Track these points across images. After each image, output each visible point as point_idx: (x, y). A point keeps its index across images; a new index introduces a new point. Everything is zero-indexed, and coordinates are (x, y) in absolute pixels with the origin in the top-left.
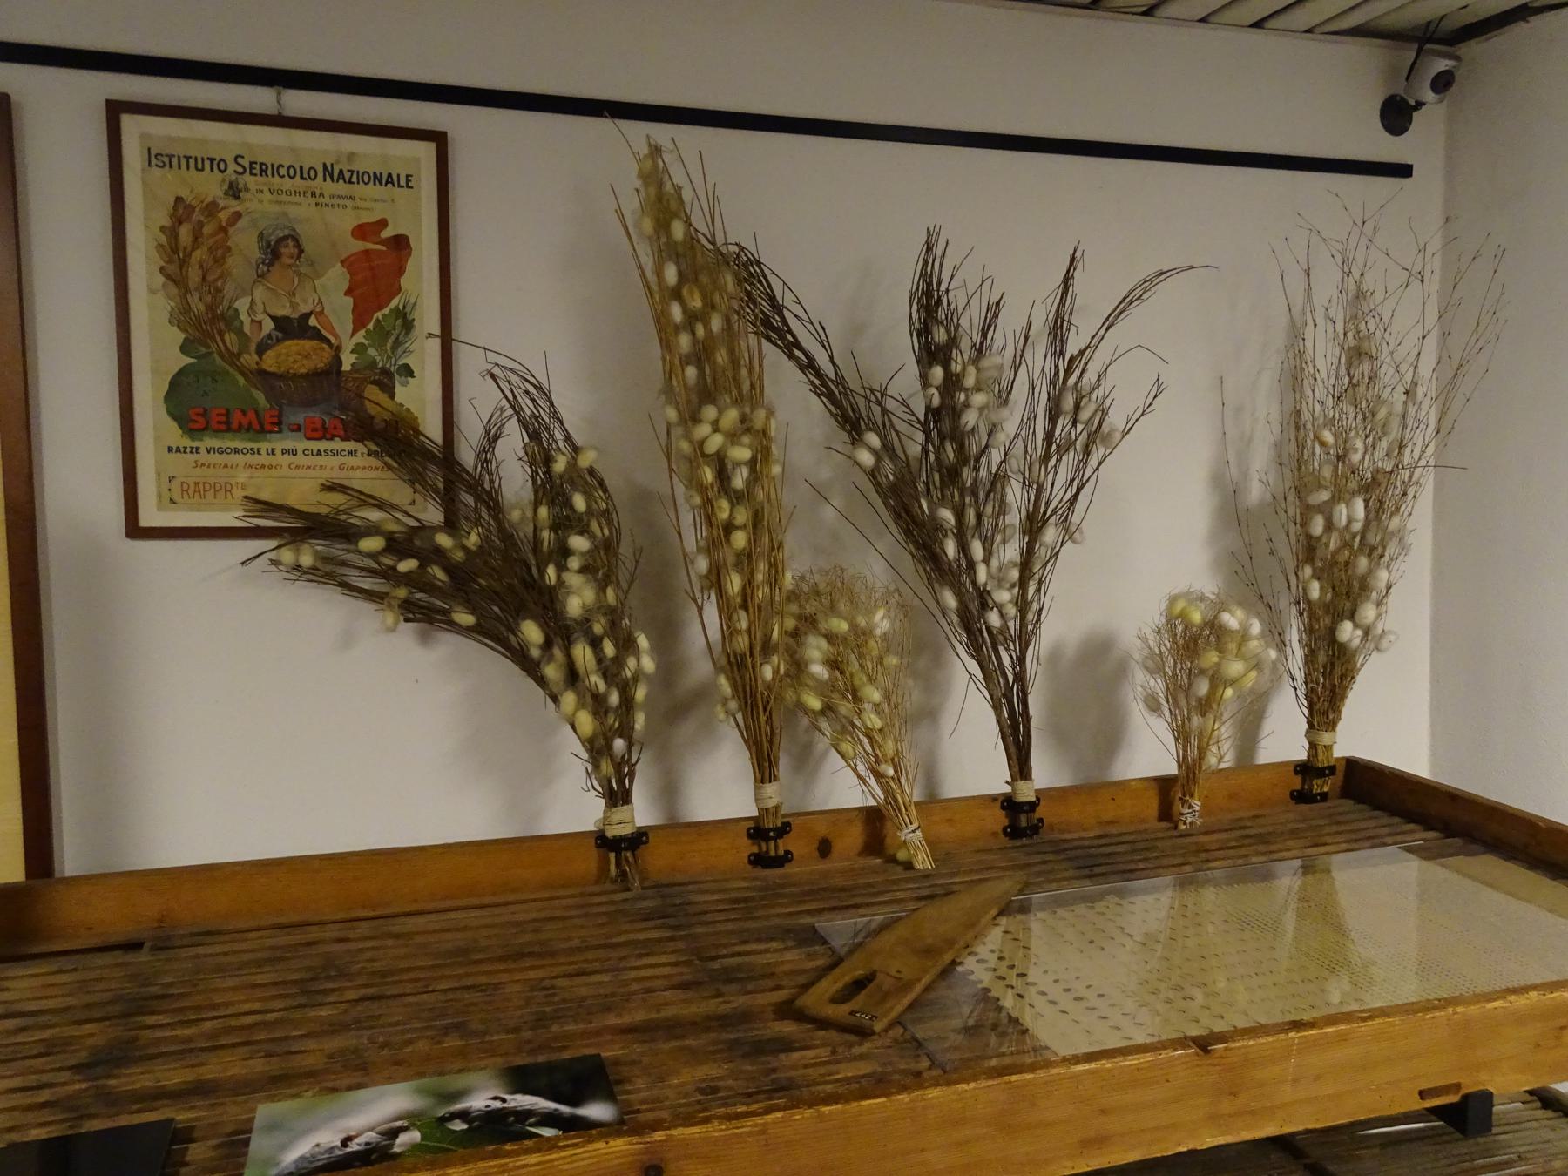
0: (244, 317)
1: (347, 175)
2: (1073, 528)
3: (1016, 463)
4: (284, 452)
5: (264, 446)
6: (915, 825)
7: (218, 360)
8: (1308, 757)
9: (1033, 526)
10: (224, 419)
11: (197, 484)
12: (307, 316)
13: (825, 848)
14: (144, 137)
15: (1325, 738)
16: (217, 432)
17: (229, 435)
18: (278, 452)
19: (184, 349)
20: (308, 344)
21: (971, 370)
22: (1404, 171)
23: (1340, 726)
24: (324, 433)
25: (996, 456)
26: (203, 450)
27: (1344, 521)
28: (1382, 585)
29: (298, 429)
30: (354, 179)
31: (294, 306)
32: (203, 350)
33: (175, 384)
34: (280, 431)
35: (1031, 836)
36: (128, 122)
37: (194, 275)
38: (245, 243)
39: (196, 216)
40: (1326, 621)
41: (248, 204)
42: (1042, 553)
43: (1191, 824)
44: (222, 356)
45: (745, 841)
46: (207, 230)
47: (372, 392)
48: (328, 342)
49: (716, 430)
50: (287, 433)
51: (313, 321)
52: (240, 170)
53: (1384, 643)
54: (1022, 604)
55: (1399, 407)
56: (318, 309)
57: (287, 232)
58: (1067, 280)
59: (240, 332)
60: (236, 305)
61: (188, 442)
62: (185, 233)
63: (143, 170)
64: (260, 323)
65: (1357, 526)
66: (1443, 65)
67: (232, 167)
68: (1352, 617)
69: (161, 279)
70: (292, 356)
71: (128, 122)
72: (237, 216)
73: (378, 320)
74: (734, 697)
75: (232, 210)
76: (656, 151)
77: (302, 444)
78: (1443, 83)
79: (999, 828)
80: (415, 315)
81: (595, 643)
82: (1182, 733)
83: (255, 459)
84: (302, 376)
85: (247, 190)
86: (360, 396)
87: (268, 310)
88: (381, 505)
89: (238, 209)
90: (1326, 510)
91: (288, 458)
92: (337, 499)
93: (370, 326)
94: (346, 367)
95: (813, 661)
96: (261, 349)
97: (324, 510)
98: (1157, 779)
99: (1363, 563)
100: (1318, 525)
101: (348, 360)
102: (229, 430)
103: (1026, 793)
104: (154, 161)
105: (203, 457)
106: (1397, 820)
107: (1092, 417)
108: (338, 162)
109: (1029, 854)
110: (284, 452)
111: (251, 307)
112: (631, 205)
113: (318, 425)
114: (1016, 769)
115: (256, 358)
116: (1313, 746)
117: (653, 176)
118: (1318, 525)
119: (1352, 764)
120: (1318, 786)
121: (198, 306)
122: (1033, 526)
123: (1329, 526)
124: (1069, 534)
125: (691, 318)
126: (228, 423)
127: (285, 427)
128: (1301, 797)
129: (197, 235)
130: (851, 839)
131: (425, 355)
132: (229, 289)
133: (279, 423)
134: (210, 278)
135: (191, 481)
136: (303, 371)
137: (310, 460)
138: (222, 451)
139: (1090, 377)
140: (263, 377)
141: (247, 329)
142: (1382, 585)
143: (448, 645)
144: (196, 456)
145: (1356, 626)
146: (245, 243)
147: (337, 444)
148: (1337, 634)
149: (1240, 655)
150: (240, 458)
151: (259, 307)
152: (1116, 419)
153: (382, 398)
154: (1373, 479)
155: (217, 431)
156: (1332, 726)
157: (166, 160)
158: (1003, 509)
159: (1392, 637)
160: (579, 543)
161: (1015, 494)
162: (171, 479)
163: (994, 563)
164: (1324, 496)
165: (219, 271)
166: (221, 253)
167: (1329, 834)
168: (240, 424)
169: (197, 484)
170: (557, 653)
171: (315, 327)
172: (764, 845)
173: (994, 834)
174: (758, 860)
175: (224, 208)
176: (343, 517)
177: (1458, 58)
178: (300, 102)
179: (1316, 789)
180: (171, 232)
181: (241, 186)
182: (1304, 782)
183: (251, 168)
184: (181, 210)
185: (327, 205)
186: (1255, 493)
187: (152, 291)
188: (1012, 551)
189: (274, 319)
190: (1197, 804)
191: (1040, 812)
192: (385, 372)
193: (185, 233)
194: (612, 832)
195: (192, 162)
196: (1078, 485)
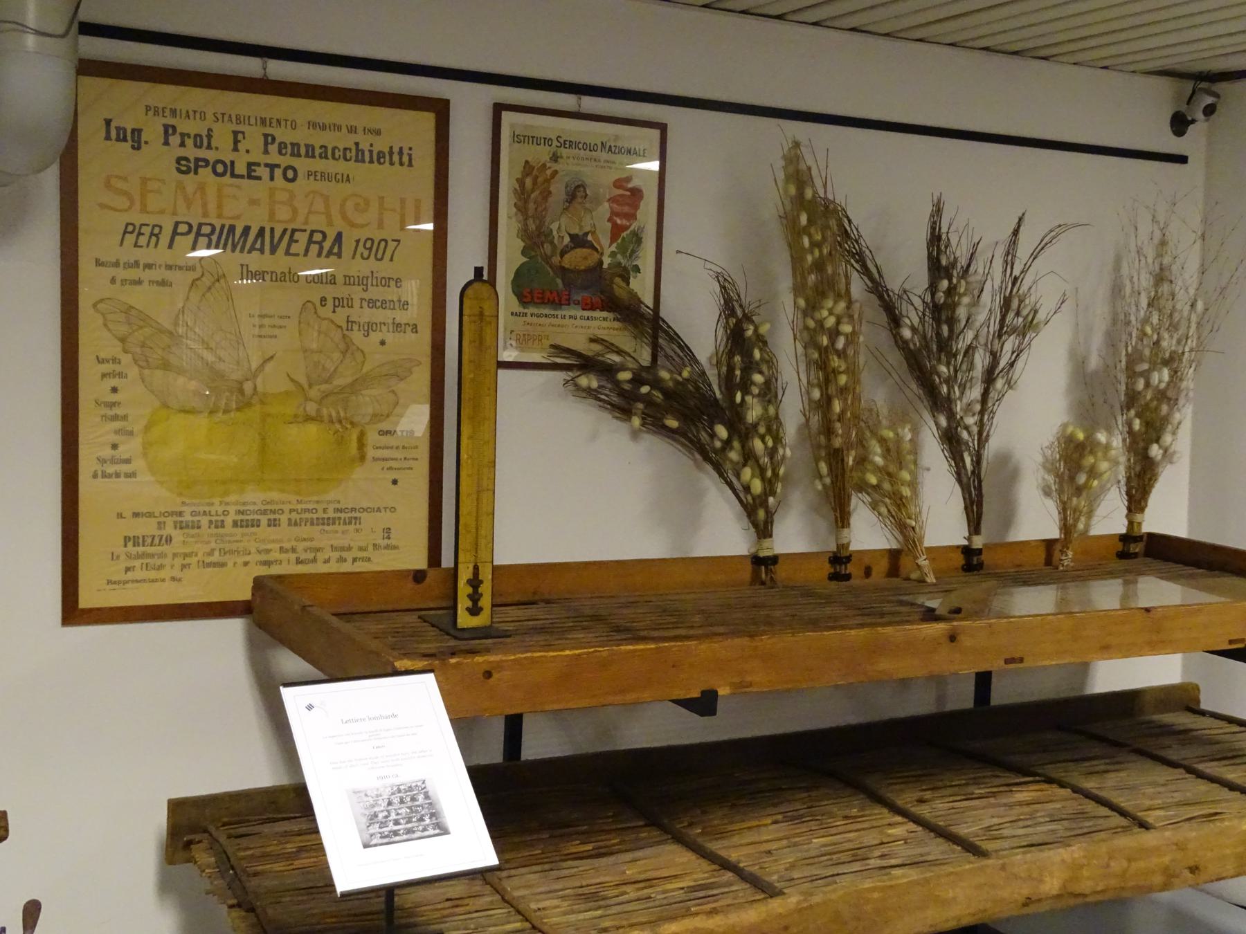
0: (555, 233)
1: (613, 149)
2: (1012, 382)
3: (982, 340)
4: (571, 317)
5: (559, 313)
6: (925, 557)
7: (540, 260)
8: (1127, 530)
9: (989, 377)
10: (540, 296)
11: (524, 335)
12: (586, 234)
13: (868, 572)
14: (512, 126)
15: (1138, 517)
16: (536, 304)
17: (543, 306)
18: (567, 317)
19: (523, 253)
20: (586, 251)
21: (963, 282)
22: (1182, 159)
23: (1147, 510)
24: (592, 308)
25: (970, 335)
26: (529, 315)
27: (1156, 382)
28: (1176, 422)
29: (578, 304)
30: (617, 151)
31: (581, 227)
32: (533, 254)
33: (518, 274)
34: (569, 304)
35: (978, 570)
36: (506, 116)
37: (531, 206)
38: (558, 190)
39: (535, 172)
40: (1141, 444)
41: (561, 166)
42: (993, 395)
43: (1067, 565)
44: (541, 257)
45: (827, 565)
46: (540, 180)
47: (618, 280)
48: (596, 250)
49: (831, 313)
50: (572, 305)
51: (590, 238)
52: (559, 145)
53: (1175, 459)
54: (981, 424)
55: (1186, 314)
56: (593, 230)
57: (580, 183)
58: (1016, 232)
59: (552, 243)
60: (551, 227)
61: (522, 310)
62: (529, 182)
63: (510, 145)
64: (563, 237)
65: (1163, 386)
66: (1209, 100)
67: (555, 143)
68: (1157, 441)
69: (515, 210)
70: (577, 259)
71: (506, 116)
72: (556, 172)
73: (624, 238)
74: (828, 475)
75: (552, 169)
76: (797, 145)
77: (580, 313)
78: (1209, 111)
79: (960, 566)
80: (644, 236)
81: (763, 438)
82: (1064, 509)
83: (554, 321)
84: (582, 271)
85: (562, 157)
86: (612, 282)
87: (568, 230)
88: (619, 352)
89: (555, 168)
90: (1146, 375)
91: (572, 321)
92: (597, 348)
93: (619, 241)
94: (605, 266)
95: (875, 454)
96: (563, 254)
97: (590, 354)
98: (1044, 541)
99: (1165, 408)
100: (1140, 384)
101: (607, 261)
102: (543, 303)
103: (978, 542)
104: (516, 139)
105: (529, 319)
106: (1181, 565)
107: (1028, 315)
108: (609, 140)
109: (639, 889)
110: (571, 317)
111: (559, 228)
112: (781, 175)
113: (589, 301)
114: (972, 528)
115: (559, 258)
116: (1131, 523)
117: (793, 158)
118: (1140, 384)
119: (1151, 536)
120: (1137, 548)
121: (532, 226)
122: (989, 377)
123: (1147, 385)
124: (1010, 384)
125: (814, 244)
126: (543, 298)
127: (571, 302)
128: (1123, 555)
129: (535, 183)
130: (881, 566)
131: (646, 259)
132: (548, 219)
133: (569, 300)
134: (540, 209)
135: (521, 334)
136: (583, 268)
137: (535, 320)
138: (538, 316)
139: (1024, 288)
140: (563, 271)
141: (556, 241)
142: (1176, 422)
143: (653, 443)
144: (524, 318)
145: (1160, 447)
146: (558, 190)
147: (597, 314)
148: (1149, 451)
149: (1106, 457)
150: (548, 321)
151: (563, 228)
152: (1041, 316)
153: (623, 284)
154: (1170, 356)
155: (536, 303)
156: (1142, 510)
157: (522, 138)
158: (971, 367)
159: (1178, 455)
160: (758, 378)
161: (981, 360)
162: (512, 331)
163: (965, 401)
164: (1145, 366)
165: (544, 206)
166: (547, 194)
167: (1040, 817)
168: (549, 299)
169: (524, 335)
170: (736, 444)
171: (591, 241)
172: (838, 567)
173: (956, 569)
174: (835, 577)
175: (549, 168)
176: (600, 358)
177: (1217, 96)
178: (590, 104)
179: (1132, 550)
180: (521, 182)
181: (559, 154)
182: (1124, 545)
183: (565, 144)
184: (528, 168)
185: (602, 167)
186: (1094, 362)
187: (510, 217)
188: (975, 393)
189: (569, 235)
190: (1070, 554)
191: (983, 557)
192: (625, 269)
193: (529, 182)
194: (762, 554)
195: (535, 140)
196: (1018, 352)
